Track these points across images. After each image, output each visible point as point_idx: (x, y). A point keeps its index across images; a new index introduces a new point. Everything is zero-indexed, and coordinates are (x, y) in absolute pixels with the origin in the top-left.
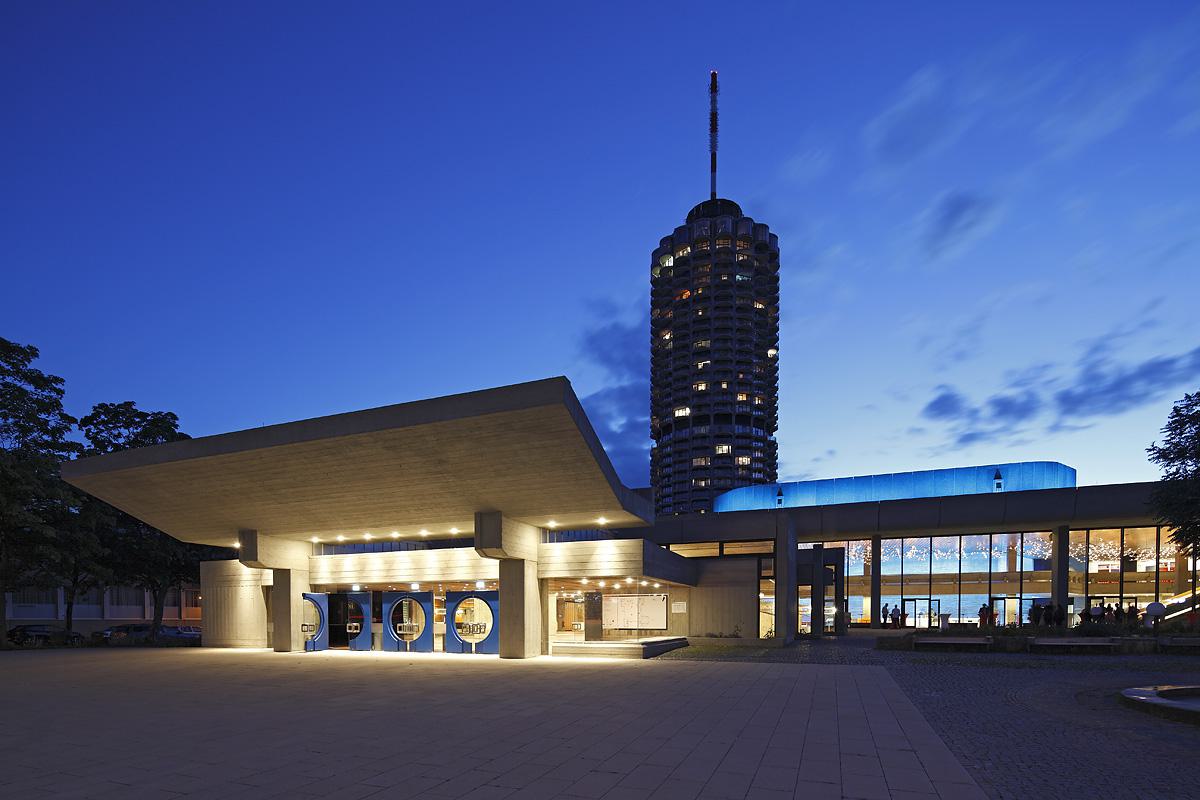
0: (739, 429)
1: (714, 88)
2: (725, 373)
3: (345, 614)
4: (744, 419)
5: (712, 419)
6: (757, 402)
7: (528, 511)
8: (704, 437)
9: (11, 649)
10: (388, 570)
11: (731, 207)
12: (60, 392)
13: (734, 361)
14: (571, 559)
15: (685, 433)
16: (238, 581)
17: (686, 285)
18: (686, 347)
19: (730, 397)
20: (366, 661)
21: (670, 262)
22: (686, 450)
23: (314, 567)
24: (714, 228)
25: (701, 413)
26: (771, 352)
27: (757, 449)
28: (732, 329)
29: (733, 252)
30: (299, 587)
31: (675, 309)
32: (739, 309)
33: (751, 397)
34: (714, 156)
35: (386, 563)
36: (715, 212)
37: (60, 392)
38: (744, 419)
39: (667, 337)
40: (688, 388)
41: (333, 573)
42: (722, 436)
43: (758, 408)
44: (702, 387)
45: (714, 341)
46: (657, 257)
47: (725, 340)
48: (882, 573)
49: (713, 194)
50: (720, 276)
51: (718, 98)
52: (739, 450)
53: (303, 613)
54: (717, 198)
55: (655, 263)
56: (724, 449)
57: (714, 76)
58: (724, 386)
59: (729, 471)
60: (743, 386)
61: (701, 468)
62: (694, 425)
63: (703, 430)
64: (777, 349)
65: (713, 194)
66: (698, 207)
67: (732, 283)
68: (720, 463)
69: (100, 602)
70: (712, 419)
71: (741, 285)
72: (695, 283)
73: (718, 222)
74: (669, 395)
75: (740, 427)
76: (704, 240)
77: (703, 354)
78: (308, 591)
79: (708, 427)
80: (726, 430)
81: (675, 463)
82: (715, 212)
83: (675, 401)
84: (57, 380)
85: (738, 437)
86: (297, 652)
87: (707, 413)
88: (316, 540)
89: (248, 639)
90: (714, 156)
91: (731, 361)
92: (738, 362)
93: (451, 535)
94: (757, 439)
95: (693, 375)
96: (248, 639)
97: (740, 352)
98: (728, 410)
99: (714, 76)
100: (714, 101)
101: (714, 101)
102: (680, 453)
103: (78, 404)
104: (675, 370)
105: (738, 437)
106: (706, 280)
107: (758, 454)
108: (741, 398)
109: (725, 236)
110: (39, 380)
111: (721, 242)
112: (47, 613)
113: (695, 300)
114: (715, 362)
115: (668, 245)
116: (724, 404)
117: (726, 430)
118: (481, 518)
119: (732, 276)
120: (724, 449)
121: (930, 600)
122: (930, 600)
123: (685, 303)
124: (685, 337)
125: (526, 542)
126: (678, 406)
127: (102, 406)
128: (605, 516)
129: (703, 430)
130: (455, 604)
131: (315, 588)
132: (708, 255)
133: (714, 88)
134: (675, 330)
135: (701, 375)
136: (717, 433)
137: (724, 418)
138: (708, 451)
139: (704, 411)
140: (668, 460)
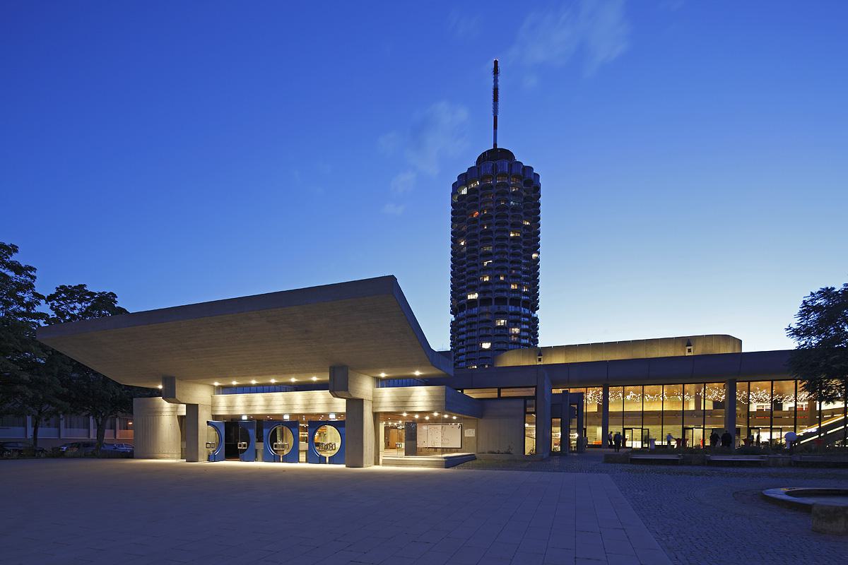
0: (512, 309)
1: (496, 71)
2: (503, 269)
7: (367, 367)
10: (268, 406)
11: (507, 155)
12: (33, 278)
14: (395, 399)
15: (475, 311)
16: (161, 412)
17: (475, 207)
21: (464, 192)
23: (215, 403)
26: (534, 255)
30: (204, 417)
35: (266, 400)
36: (496, 159)
37: (33, 278)
38: (515, 302)
39: (462, 243)
41: (228, 407)
42: (500, 313)
43: (525, 294)
44: (487, 279)
46: (456, 187)
47: (503, 246)
49: (495, 145)
53: (207, 435)
57: (496, 62)
65: (495, 145)
71: (514, 209)
72: (482, 206)
74: (463, 284)
76: (488, 177)
77: (487, 255)
80: (503, 308)
82: (496, 159)
83: (468, 288)
86: (203, 462)
89: (169, 456)
94: (525, 316)
97: (513, 255)
98: (505, 294)
99: (496, 62)
100: (496, 80)
101: (496, 80)
103: (45, 285)
107: (525, 327)
113: (484, 218)
114: (496, 261)
116: (502, 291)
117: (503, 308)
118: (333, 371)
119: (508, 201)
123: (475, 220)
125: (366, 387)
126: (472, 291)
127: (62, 287)
128: (275, 379)
130: (314, 430)
133: (496, 71)
135: (486, 270)
137: (501, 301)
139: (488, 296)
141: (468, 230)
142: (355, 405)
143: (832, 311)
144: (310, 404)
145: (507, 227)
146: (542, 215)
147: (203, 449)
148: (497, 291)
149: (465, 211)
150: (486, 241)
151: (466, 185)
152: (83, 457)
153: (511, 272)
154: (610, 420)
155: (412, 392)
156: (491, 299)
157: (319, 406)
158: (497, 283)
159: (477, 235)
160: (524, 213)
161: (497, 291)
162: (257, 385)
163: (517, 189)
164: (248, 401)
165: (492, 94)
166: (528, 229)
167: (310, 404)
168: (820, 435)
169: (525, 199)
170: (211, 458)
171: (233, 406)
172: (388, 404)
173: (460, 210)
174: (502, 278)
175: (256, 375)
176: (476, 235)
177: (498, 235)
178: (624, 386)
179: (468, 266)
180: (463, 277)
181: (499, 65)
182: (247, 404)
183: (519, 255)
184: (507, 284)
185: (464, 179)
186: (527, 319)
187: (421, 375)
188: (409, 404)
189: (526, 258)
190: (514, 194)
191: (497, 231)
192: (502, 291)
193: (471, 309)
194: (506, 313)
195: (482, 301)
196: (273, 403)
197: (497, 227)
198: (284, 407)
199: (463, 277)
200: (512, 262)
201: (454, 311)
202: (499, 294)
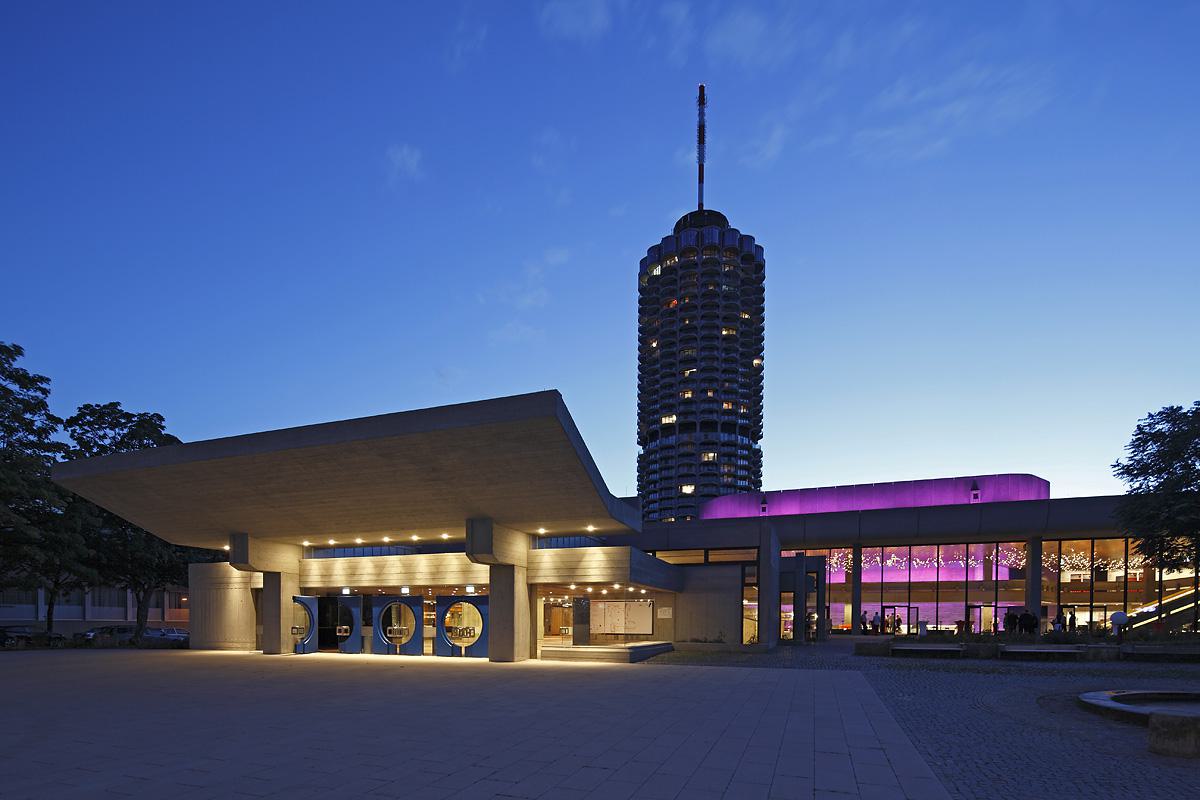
7: (520, 519)
10: (379, 575)
11: (718, 219)
14: (559, 565)
16: (228, 583)
21: (657, 271)
23: (305, 570)
35: (376, 567)
41: (322, 576)
49: (701, 205)
57: (702, 88)
65: (701, 205)
82: (703, 225)
93: (588, 532)
99: (702, 88)
100: (701, 114)
101: (701, 114)
123: (673, 312)
125: (518, 549)
142: (503, 573)
143: (1178, 440)
144: (438, 572)
145: (717, 322)
146: (766, 304)
151: (660, 262)
152: (116, 648)
155: (583, 555)
157: (452, 575)
159: (675, 333)
160: (742, 302)
162: (363, 546)
164: (350, 568)
166: (746, 325)
167: (438, 572)
171: (331, 575)
172: (547, 573)
181: (706, 92)
182: (349, 571)
185: (656, 254)
188: (579, 572)
190: (727, 274)
191: (703, 327)
196: (386, 571)
197: (703, 322)
198: (374, 578)
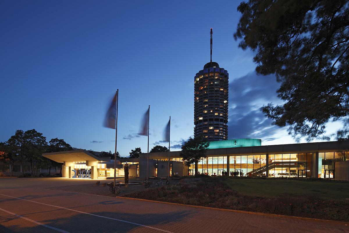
0: (215, 122)
1: (211, 33)
2: (212, 108)
3: (79, 172)
4: (217, 120)
5: (208, 120)
6: (221, 115)
8: (206, 125)
9: (38, 177)
11: (216, 64)
12: (46, 139)
13: (214, 105)
15: (202, 124)
17: (202, 86)
18: (202, 101)
19: (213, 114)
20: (75, 179)
21: (198, 80)
22: (202, 128)
24: (209, 71)
25: (205, 119)
26: (225, 102)
27: (221, 127)
28: (213, 96)
29: (214, 76)
30: (72, 169)
31: (199, 92)
32: (216, 91)
33: (219, 114)
34: (211, 50)
36: (211, 66)
37: (46, 139)
38: (217, 120)
39: (198, 99)
40: (202, 112)
42: (210, 125)
43: (221, 116)
44: (206, 112)
45: (209, 100)
46: (195, 78)
47: (212, 99)
48: (230, 163)
49: (211, 60)
50: (211, 83)
51: (213, 35)
52: (216, 128)
53: (73, 173)
54: (212, 62)
55: (195, 80)
56: (211, 128)
57: (211, 29)
58: (211, 111)
59: (212, 133)
60: (216, 111)
61: (205, 133)
62: (204, 122)
63: (206, 123)
64: (228, 101)
65: (211, 60)
66: (206, 65)
67: (214, 84)
68: (210, 132)
69: (56, 169)
70: (208, 120)
71: (216, 85)
72: (204, 85)
73: (210, 69)
74: (198, 114)
75: (216, 122)
76: (206, 74)
77: (206, 103)
78: (74, 170)
79: (207, 122)
80: (212, 123)
81: (199, 132)
82: (211, 66)
83: (199, 115)
84: (45, 137)
85: (215, 125)
86: (72, 178)
87: (207, 118)
88: (77, 162)
89: (66, 177)
90: (211, 50)
91: (213, 105)
92: (215, 105)
94: (221, 125)
95: (203, 109)
96: (66, 177)
97: (216, 102)
98: (213, 117)
99: (211, 29)
100: (211, 36)
101: (211, 36)
102: (200, 129)
103: (48, 140)
104: (199, 108)
105: (215, 125)
106: (207, 84)
107: (221, 129)
108: (216, 114)
109: (212, 72)
110: (42, 137)
111: (211, 74)
112: (46, 171)
113: (204, 89)
114: (209, 105)
115: (198, 75)
116: (212, 116)
117: (212, 123)
118: (87, 161)
119: (214, 83)
120: (211, 128)
121: (241, 170)
122: (241, 170)
123: (202, 90)
124: (202, 99)
126: (200, 117)
127: (52, 139)
129: (206, 123)
131: (75, 169)
132: (207, 78)
133: (211, 33)
134: (199, 97)
135: (205, 109)
136: (210, 124)
137: (211, 120)
138: (207, 128)
139: (206, 118)
140: (198, 131)
141: (199, 94)
147: (72, 176)
148: (210, 116)
149: (198, 87)
150: (206, 98)
153: (215, 109)
154: (230, 166)
156: (207, 119)
158: (210, 113)
161: (210, 116)
163: (218, 77)
165: (210, 41)
168: (302, 176)
169: (221, 80)
170: (73, 177)
173: (197, 86)
174: (211, 111)
175: (77, 162)
176: (202, 96)
177: (210, 95)
178: (235, 156)
179: (199, 108)
180: (198, 111)
183: (218, 102)
184: (213, 113)
186: (222, 126)
187: (253, 132)
189: (222, 103)
192: (212, 116)
193: (200, 123)
194: (213, 124)
195: (204, 120)
199: (198, 111)
200: (215, 105)
201: (195, 123)
202: (211, 117)
